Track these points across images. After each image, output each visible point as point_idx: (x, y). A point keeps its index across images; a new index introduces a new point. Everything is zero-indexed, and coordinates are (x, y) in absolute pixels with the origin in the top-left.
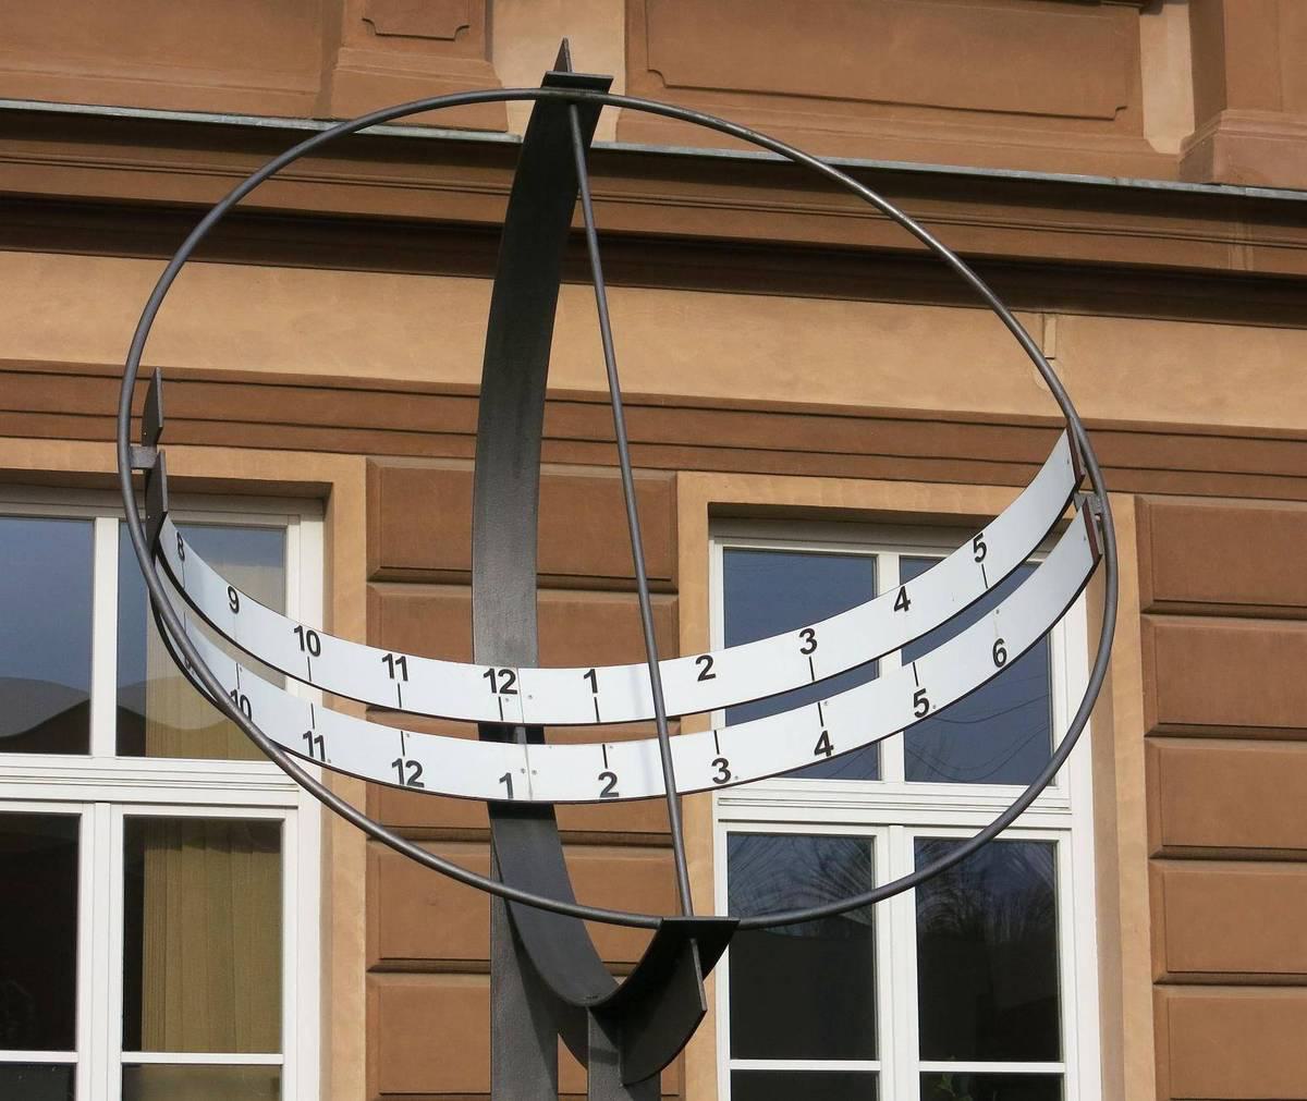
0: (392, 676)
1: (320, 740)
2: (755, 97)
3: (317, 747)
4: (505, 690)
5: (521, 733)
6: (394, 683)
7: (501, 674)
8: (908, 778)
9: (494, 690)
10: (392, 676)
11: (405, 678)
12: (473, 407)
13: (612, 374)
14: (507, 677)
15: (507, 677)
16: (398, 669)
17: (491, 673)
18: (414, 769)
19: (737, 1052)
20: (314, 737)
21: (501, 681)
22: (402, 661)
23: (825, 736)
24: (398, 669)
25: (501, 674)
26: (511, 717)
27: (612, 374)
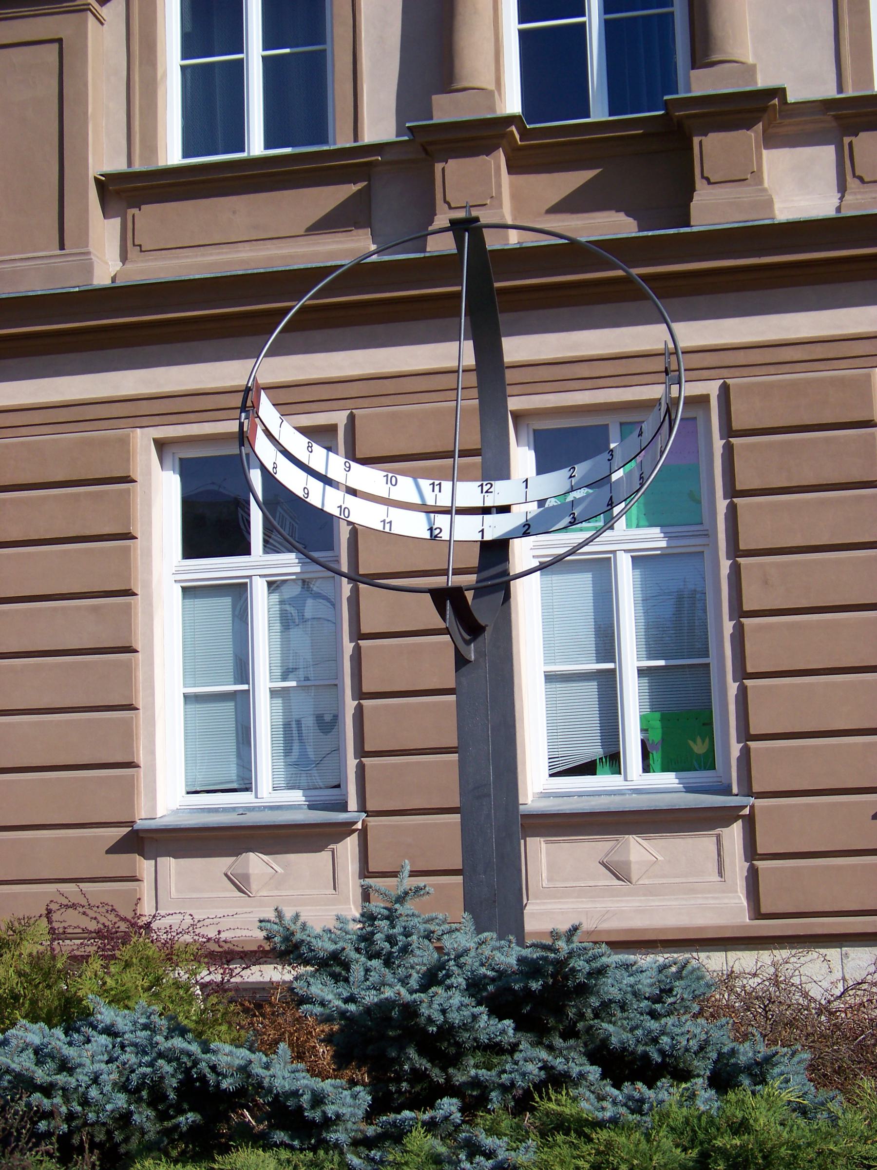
0: (433, 491)
1: (390, 522)
2: (722, 185)
3: (387, 526)
4: (487, 492)
5: (494, 510)
6: (434, 494)
7: (486, 485)
8: (248, 553)
9: (482, 492)
10: (433, 491)
11: (440, 491)
12: (476, 390)
13: (323, 504)
14: (489, 486)
15: (489, 486)
16: (437, 488)
17: (482, 485)
18: (438, 531)
19: (245, 550)
20: (386, 522)
21: (485, 488)
22: (440, 484)
23: (611, 497)
24: (437, 488)
25: (486, 485)
26: (489, 503)
27: (323, 504)
